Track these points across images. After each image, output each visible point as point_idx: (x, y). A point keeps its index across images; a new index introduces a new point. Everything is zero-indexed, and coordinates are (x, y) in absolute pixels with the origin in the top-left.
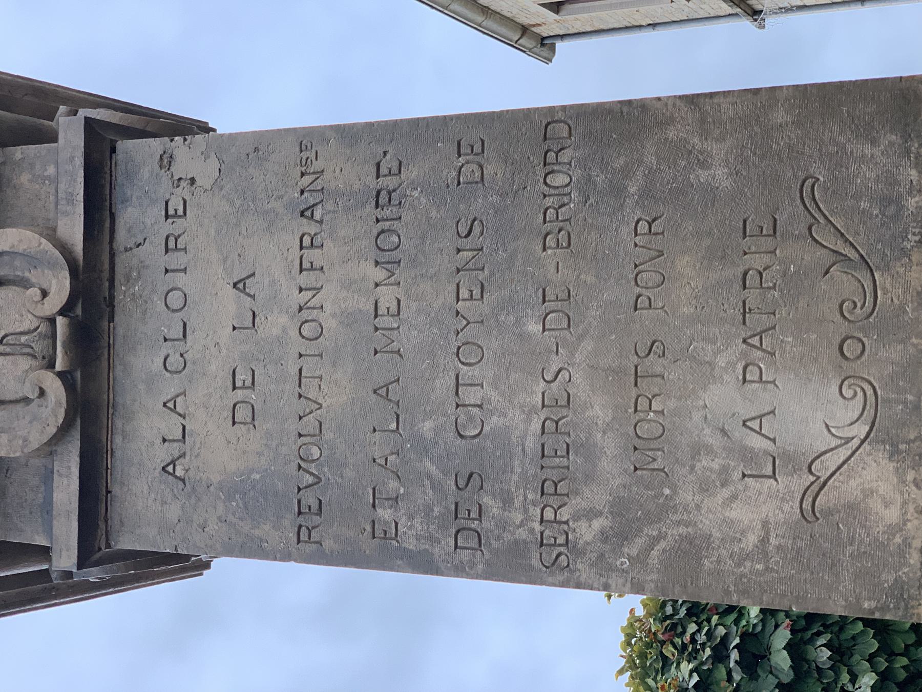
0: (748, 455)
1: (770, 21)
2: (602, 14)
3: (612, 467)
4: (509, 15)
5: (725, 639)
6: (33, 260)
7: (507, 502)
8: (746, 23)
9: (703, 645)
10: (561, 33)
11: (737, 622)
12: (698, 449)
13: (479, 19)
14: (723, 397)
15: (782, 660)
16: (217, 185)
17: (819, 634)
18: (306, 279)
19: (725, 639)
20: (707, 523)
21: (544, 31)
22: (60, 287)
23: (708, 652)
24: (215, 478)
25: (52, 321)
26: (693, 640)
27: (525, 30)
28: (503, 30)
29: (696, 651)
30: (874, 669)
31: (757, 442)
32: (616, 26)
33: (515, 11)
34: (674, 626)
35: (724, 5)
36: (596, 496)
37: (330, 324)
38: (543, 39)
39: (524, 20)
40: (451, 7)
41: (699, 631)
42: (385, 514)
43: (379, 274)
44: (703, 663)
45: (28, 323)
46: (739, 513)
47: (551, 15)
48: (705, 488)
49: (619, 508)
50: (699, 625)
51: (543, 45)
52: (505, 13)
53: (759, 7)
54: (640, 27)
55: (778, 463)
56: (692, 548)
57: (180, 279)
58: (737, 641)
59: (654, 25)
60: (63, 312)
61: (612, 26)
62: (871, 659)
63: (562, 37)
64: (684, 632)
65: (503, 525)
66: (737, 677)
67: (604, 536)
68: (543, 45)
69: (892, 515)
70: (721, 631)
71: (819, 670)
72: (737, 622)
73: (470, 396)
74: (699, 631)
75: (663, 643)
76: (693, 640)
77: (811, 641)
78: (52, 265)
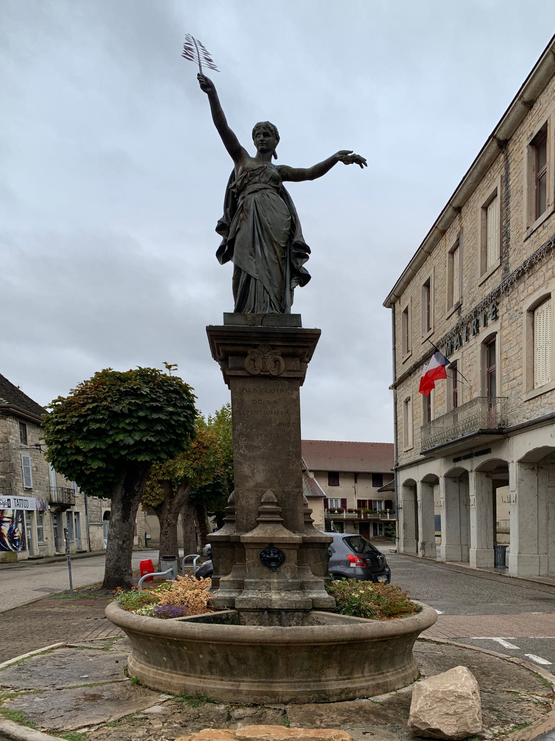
0: (254, 470)
1: (392, 391)
2: (401, 330)
3: (250, 454)
4: (405, 292)
5: (159, 401)
6: (279, 369)
7: (245, 441)
8: (391, 382)
9: (156, 395)
10: (396, 312)
11: (165, 404)
12: (254, 465)
13: (404, 280)
14: (261, 467)
15: (155, 416)
16: (292, 398)
17: (165, 427)
18: (276, 412)
19: (159, 401)
20: (244, 465)
21: (397, 305)
22: (274, 373)
23: (154, 397)
24: (244, 397)
25: (269, 372)
26: (157, 392)
27: (398, 297)
28: (398, 289)
29: (154, 393)
30: (157, 441)
31: (255, 471)
32: (396, 334)
33: (407, 294)
34: (160, 386)
35: (400, 376)
36: (246, 452)
37: (269, 416)
38: (394, 304)
39: (403, 297)
40: (410, 269)
41: (160, 393)
42: (241, 424)
43: (277, 423)
44: (150, 395)
45: (268, 368)
46: (246, 469)
47: (403, 309)
48: (249, 465)
49: (245, 455)
50: (162, 393)
51: (391, 304)
52: (406, 290)
53: (398, 388)
54: (394, 343)
55: (253, 474)
56: (241, 463)
57: (276, 392)
58: (159, 405)
59: (394, 349)
60: (270, 374)
61: (396, 332)
62: (159, 440)
63: (394, 312)
64: (158, 388)
65: (241, 440)
66: (147, 404)
67: (241, 453)
68: (391, 304)
69: (248, 485)
70: (162, 400)
71: (153, 427)
72: (165, 404)
73: (259, 436)
74: (160, 393)
75: (154, 382)
76: (157, 392)
77: (162, 425)
78: (278, 373)
